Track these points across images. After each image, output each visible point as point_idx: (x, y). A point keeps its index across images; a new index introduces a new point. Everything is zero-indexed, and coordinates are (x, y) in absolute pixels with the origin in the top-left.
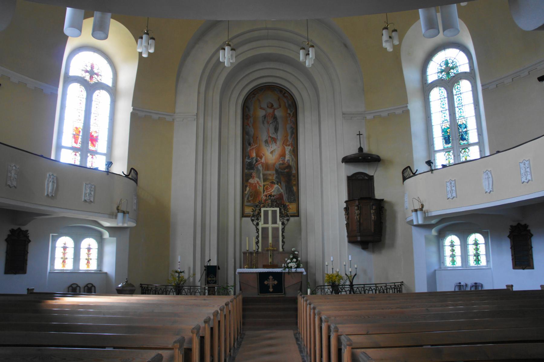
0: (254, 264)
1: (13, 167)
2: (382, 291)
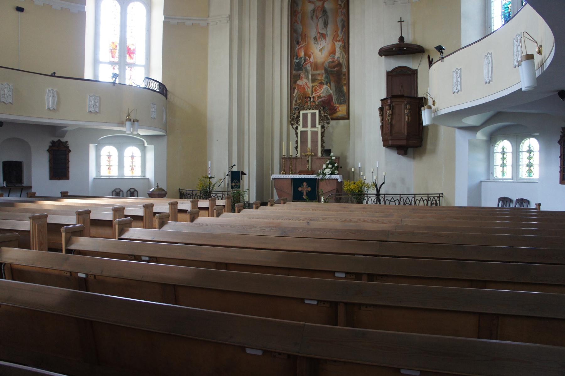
1: (5, 85)
2: (434, 202)
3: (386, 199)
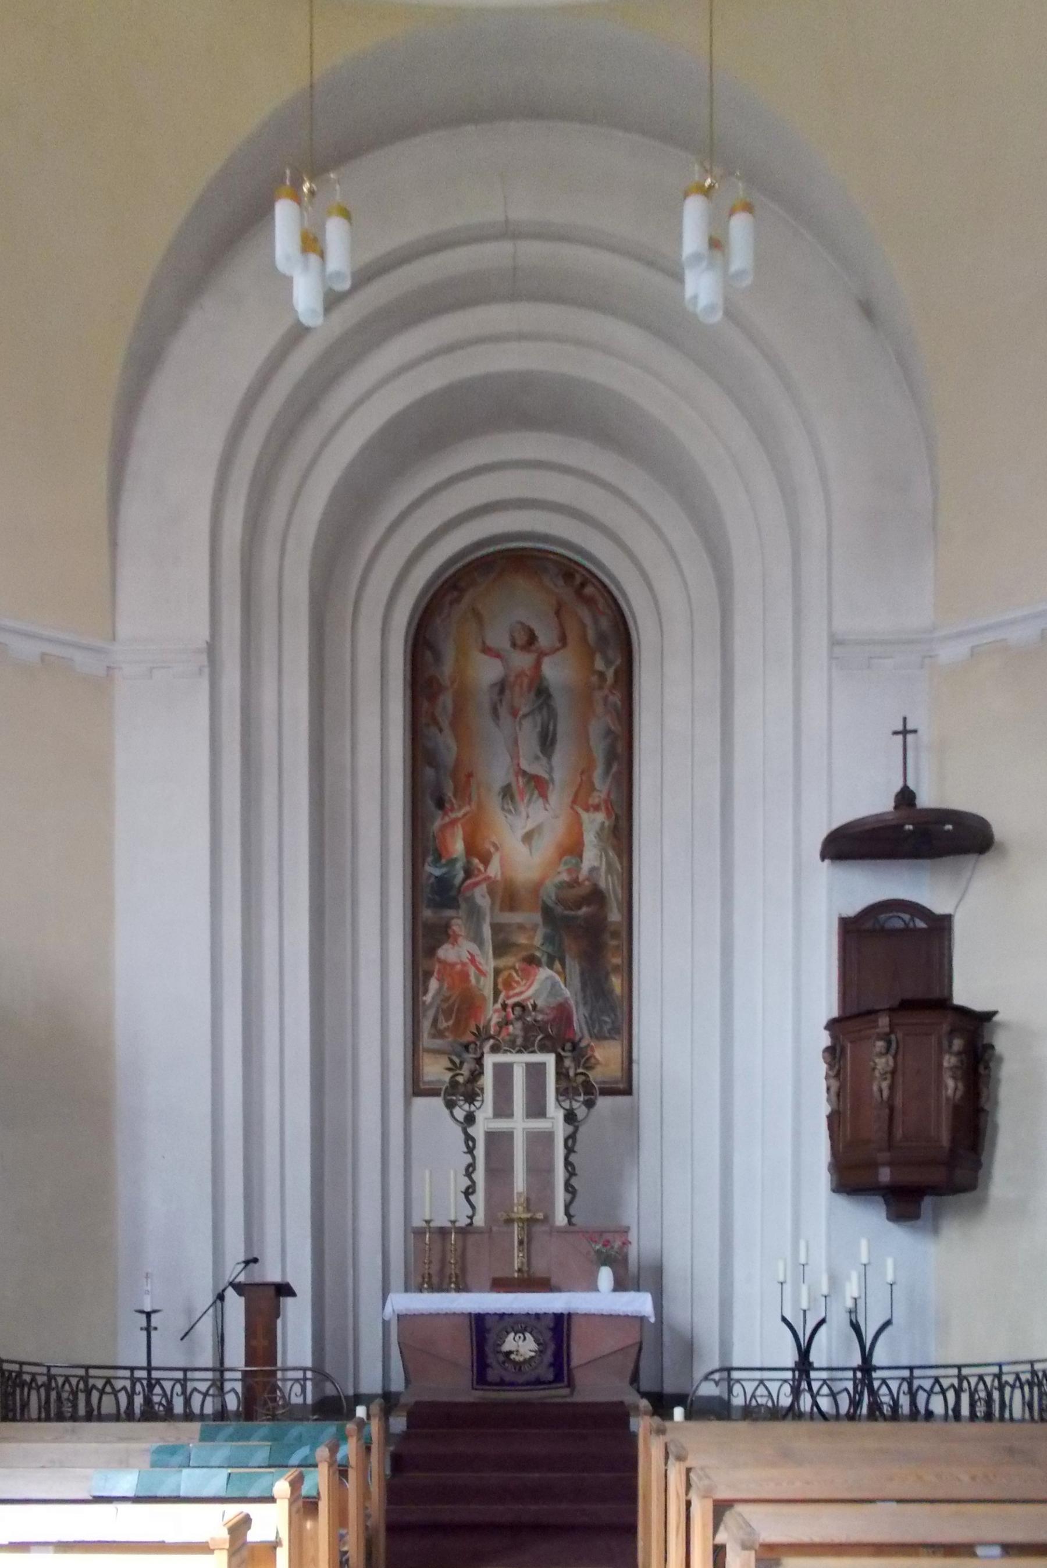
0: (450, 1278)
2: (983, 1394)
3: (190, 1386)
